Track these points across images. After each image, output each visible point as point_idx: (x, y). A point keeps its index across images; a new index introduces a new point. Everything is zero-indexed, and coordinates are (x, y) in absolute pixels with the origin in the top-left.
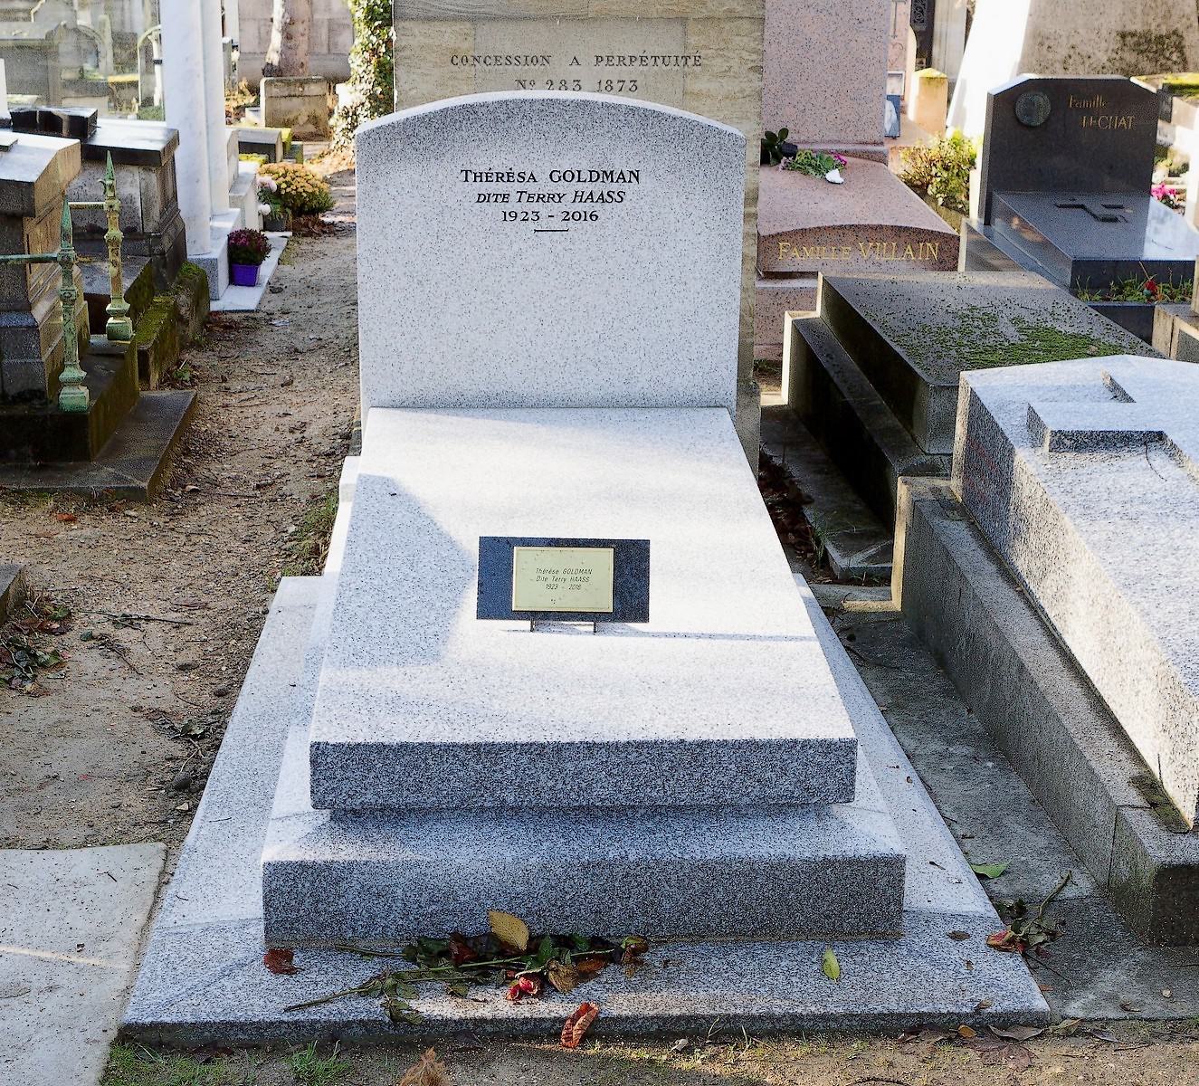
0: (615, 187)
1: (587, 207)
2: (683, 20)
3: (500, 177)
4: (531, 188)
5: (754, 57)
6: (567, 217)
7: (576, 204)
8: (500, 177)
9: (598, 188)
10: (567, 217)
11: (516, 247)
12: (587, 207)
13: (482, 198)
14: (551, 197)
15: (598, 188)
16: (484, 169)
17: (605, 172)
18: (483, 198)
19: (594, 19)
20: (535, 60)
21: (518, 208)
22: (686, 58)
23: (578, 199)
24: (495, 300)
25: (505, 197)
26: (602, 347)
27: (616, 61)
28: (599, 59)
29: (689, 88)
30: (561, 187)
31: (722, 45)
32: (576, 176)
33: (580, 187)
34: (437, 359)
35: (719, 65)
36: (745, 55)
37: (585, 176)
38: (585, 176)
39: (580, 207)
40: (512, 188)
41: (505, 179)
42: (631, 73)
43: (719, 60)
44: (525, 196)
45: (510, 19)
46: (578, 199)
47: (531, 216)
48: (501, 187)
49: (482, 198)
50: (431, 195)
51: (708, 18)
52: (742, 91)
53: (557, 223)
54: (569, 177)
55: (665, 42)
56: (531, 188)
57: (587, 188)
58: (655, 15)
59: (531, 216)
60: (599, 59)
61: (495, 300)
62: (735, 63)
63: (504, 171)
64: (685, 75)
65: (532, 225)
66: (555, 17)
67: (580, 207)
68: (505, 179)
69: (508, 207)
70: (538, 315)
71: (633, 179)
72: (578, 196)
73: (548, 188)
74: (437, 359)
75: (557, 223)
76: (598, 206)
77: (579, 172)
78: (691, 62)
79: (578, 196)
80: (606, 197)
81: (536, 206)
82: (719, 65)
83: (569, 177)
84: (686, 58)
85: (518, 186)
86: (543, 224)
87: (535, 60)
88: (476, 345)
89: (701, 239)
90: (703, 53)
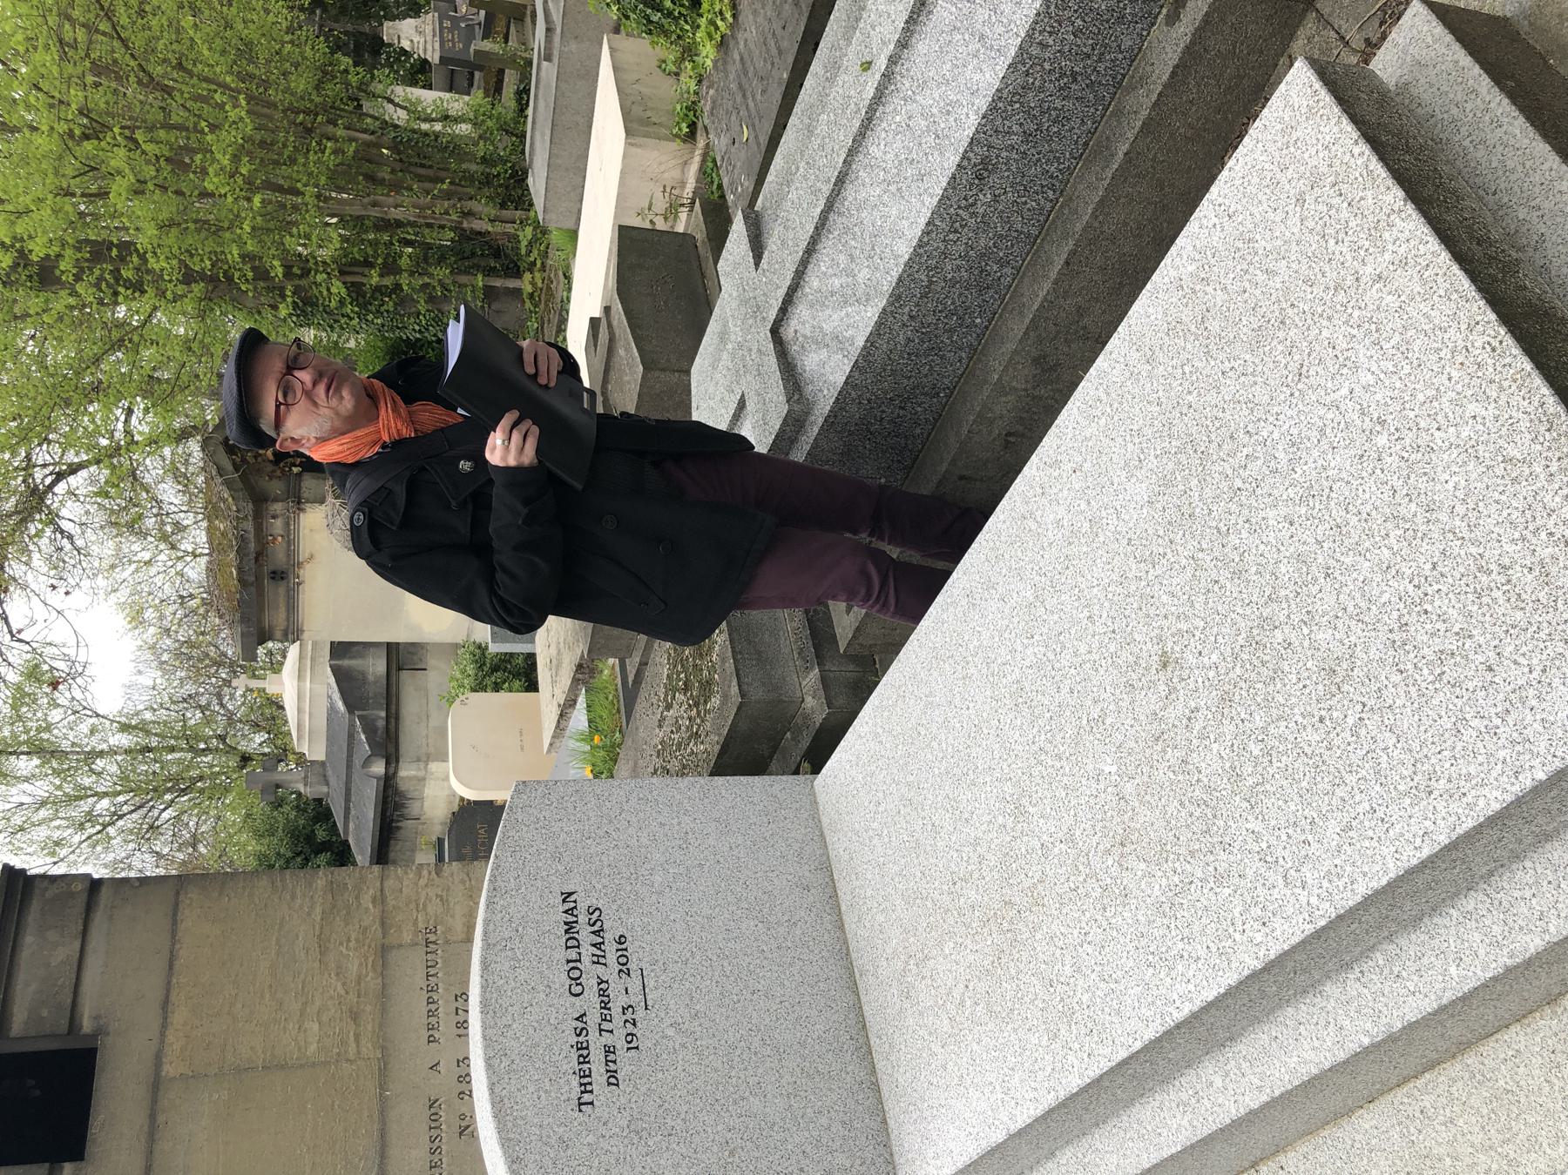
0: (583, 919)
1: (611, 949)
2: (384, 950)
3: (583, 1060)
4: (593, 1019)
5: (425, 873)
6: (625, 971)
7: (608, 961)
8: (583, 1060)
9: (585, 935)
10: (625, 971)
11: (670, 1032)
12: (611, 949)
13: (613, 1080)
14: (603, 993)
15: (585, 935)
16: (575, 1081)
17: (567, 932)
18: (613, 1078)
19: (383, 1048)
20: (434, 1117)
21: (620, 1033)
22: (427, 943)
23: (602, 960)
24: (738, 1052)
25: (609, 1050)
26: (773, 919)
27: (433, 1020)
28: (431, 1040)
29: (462, 936)
30: (590, 982)
31: (413, 906)
32: (574, 964)
33: (586, 959)
34: (824, 1121)
35: (434, 908)
36: (422, 882)
37: (573, 954)
38: (573, 954)
39: (611, 957)
40: (596, 1042)
41: (585, 1052)
42: (447, 1001)
43: (429, 909)
44: (605, 1026)
45: (383, 1155)
46: (602, 960)
47: (629, 1016)
48: (597, 1056)
49: (613, 1080)
50: (615, 1150)
51: (383, 924)
52: (463, 882)
53: (634, 983)
54: (576, 974)
55: (410, 969)
56: (593, 1019)
57: (587, 951)
58: (379, 980)
59: (629, 1016)
60: (431, 1040)
61: (738, 1052)
62: (432, 892)
63: (574, 1055)
64: (447, 942)
65: (640, 1013)
66: (383, 1100)
67: (611, 957)
68: (585, 1052)
69: (621, 1044)
70: (749, 996)
71: (572, 898)
72: (598, 961)
73: (591, 998)
74: (824, 1121)
75: (634, 983)
76: (608, 936)
77: (569, 961)
78: (432, 938)
79: (598, 961)
80: (596, 928)
81: (616, 1009)
82: (434, 908)
83: (576, 974)
84: (427, 943)
85: (593, 1035)
86: (636, 999)
87: (434, 1117)
88: (798, 1070)
89: (634, 819)
90: (421, 925)
